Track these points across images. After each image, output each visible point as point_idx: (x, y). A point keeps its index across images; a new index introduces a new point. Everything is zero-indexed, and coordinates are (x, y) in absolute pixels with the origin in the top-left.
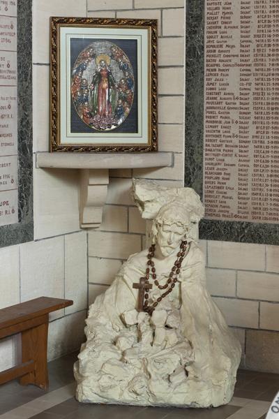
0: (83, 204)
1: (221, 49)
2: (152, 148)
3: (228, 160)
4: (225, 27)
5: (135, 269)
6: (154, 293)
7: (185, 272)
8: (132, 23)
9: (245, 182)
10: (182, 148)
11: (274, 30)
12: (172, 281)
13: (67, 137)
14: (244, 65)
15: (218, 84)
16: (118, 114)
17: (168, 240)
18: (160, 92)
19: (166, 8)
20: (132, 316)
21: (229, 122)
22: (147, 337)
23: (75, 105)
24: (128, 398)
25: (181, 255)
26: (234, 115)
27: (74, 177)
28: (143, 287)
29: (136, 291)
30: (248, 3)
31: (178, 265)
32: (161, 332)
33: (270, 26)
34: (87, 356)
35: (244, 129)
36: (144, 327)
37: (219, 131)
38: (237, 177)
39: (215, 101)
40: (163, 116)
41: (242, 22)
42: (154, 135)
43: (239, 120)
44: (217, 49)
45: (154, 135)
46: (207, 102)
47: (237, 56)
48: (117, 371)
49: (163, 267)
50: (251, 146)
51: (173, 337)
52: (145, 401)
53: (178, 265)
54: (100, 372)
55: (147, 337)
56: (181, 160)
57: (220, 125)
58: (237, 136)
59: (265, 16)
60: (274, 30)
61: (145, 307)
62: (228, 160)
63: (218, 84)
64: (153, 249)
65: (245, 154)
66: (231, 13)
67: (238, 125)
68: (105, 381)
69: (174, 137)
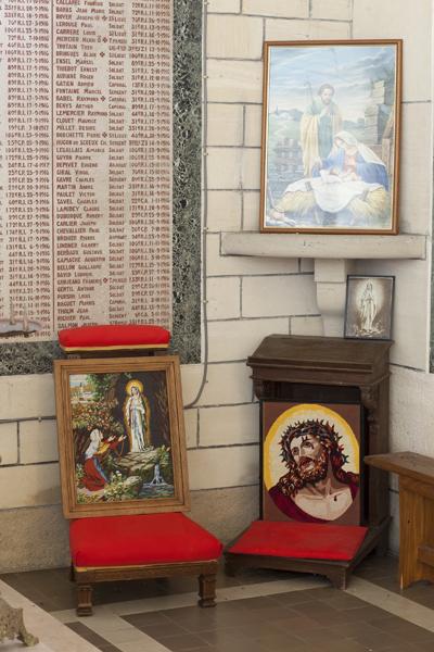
1: (79, 154)
4: (88, 150)
9: (119, 255)
11: (158, 214)
14: (116, 220)
15: (78, 69)
19: (13, 465)
21: (93, 41)
30: (121, 5)
33: (153, 93)
37: (74, 187)
38: (107, 219)
39: (67, 279)
41: (111, 252)
43: (108, 132)
44: (78, 235)
46: (59, 186)
47: (104, 114)
50: (128, 286)
57: (75, 286)
58: (105, 40)
59: (146, 271)
60: (158, 214)
63: (78, 69)
65: (119, 74)
66: (92, 180)
67: (108, 22)
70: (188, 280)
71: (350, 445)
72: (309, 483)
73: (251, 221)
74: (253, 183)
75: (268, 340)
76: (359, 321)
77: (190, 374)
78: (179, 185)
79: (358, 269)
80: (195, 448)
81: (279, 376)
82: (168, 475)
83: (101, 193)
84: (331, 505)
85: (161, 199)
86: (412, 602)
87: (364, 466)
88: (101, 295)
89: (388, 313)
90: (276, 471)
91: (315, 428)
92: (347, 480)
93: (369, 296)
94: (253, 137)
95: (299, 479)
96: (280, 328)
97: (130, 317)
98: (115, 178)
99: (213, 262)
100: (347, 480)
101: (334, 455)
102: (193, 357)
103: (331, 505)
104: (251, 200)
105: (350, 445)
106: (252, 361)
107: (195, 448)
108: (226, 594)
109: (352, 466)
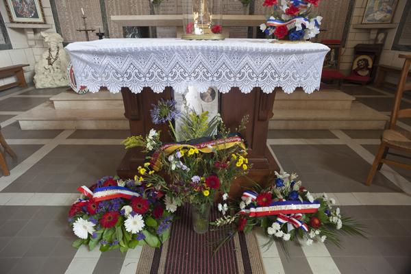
0: (28, 40)
2: (45, 23)
3: (68, 26)
5: (46, 55)
6: (52, 60)
7: (60, 55)
8: (43, 15)
10: (54, 23)
12: (57, 57)
13: (15, 19)
16: (31, 12)
17: (53, 46)
18: (45, 15)
20: (47, 67)
22: (52, 71)
23: (16, 9)
24: (50, 86)
25: (58, 51)
26: (66, 13)
27: (21, 31)
28: (49, 59)
29: (47, 61)
31: (58, 53)
32: (56, 70)
34: (44, 65)
35: (70, 18)
36: (51, 69)
40: (46, 14)
42: (44, 19)
45: (44, 19)
48: (46, 80)
49: (54, 54)
51: (59, 70)
52: (55, 86)
53: (58, 53)
54: (41, 81)
55: (52, 71)
56: (54, 26)
61: (50, 64)
62: (68, 26)
64: (50, 49)
68: (42, 82)
69: (50, 20)
70: (346, 32)
71: (370, 63)
72: (361, 69)
73: (360, 22)
74: (362, 15)
75: (359, 45)
76: (378, 41)
77: (343, 49)
78: (348, 15)
79: (380, 30)
80: (393, 17)
81: (359, 50)
82: (336, 65)
83: (333, 17)
84: (365, 73)
85: (344, 19)
86: (369, 108)
87: (373, 66)
88: (161, 89)
89: (384, 40)
90: (355, 67)
91: (364, 60)
92: (368, 69)
93: (381, 36)
94: (364, 6)
95: (359, 68)
96: (361, 42)
97: (334, 38)
98: (336, 13)
99: (351, 29)
100: (368, 69)
101: (367, 64)
102: (344, 47)
103: (365, 73)
104: (361, 19)
105: (370, 63)
106: (355, 48)
107: (393, 17)
108: (343, 85)
109: (370, 67)
